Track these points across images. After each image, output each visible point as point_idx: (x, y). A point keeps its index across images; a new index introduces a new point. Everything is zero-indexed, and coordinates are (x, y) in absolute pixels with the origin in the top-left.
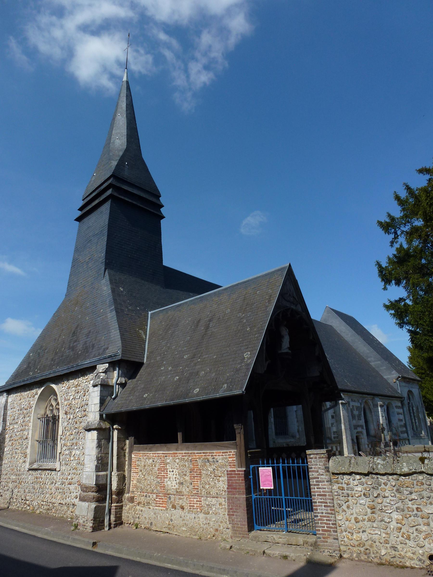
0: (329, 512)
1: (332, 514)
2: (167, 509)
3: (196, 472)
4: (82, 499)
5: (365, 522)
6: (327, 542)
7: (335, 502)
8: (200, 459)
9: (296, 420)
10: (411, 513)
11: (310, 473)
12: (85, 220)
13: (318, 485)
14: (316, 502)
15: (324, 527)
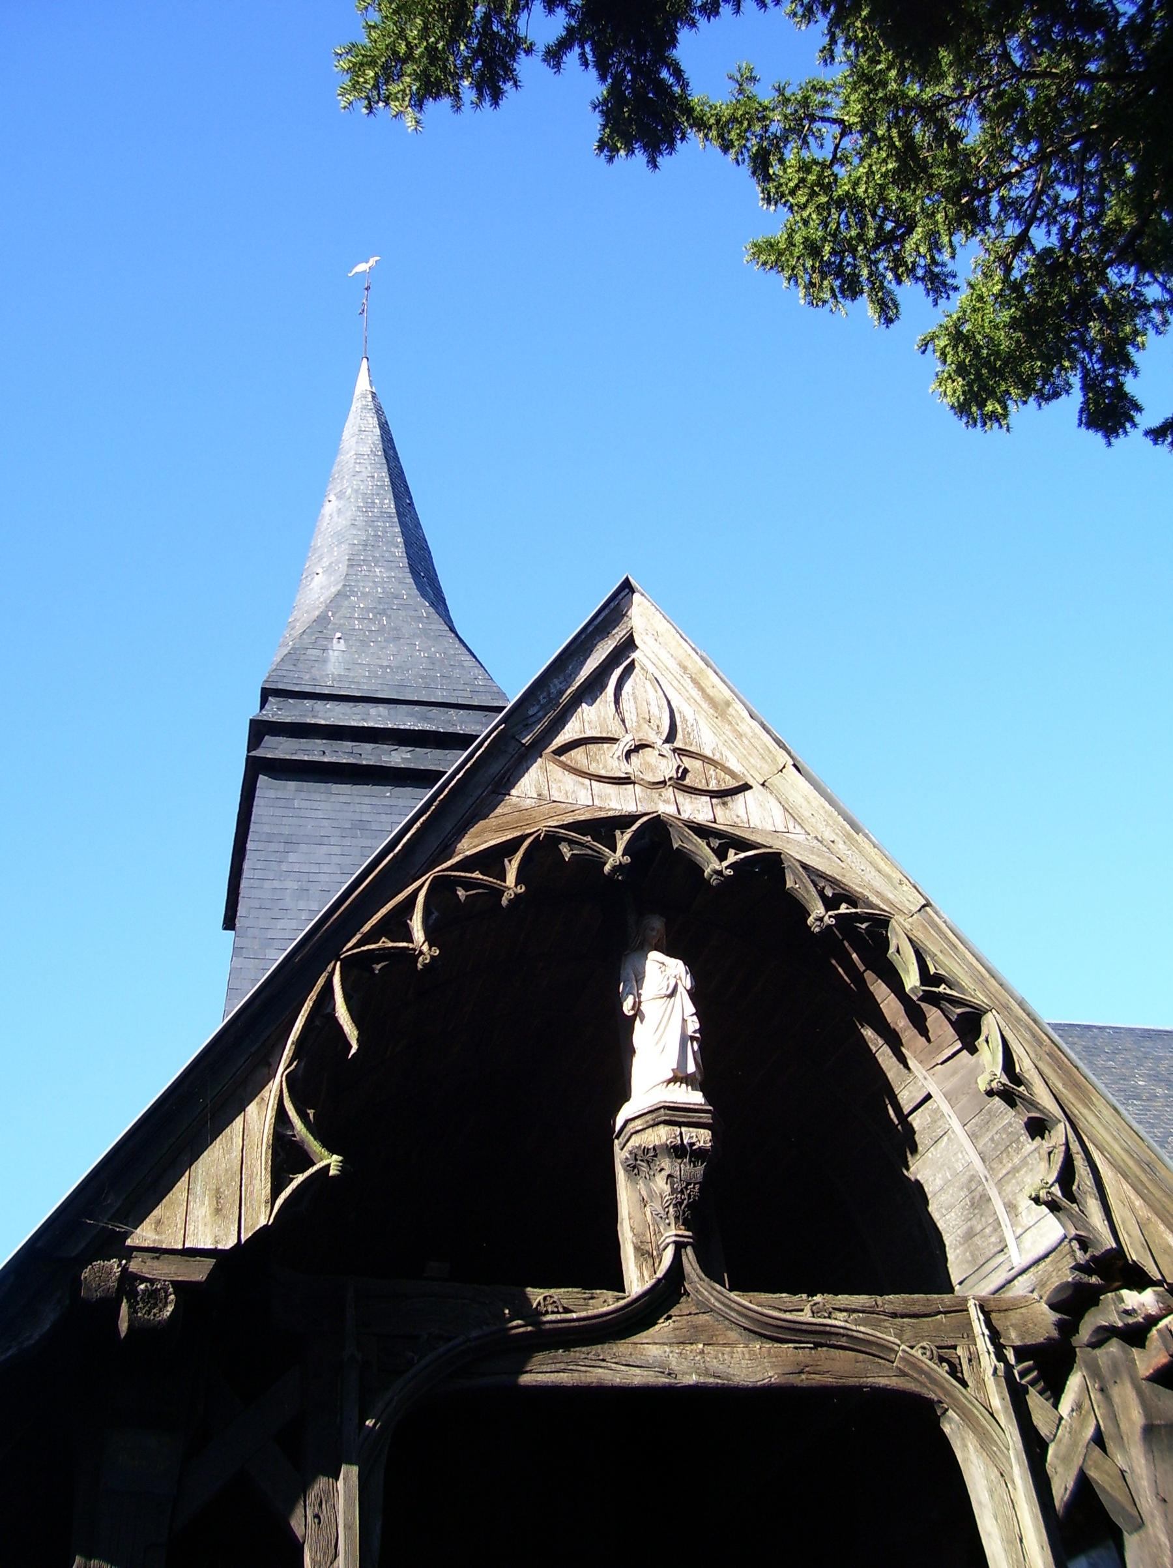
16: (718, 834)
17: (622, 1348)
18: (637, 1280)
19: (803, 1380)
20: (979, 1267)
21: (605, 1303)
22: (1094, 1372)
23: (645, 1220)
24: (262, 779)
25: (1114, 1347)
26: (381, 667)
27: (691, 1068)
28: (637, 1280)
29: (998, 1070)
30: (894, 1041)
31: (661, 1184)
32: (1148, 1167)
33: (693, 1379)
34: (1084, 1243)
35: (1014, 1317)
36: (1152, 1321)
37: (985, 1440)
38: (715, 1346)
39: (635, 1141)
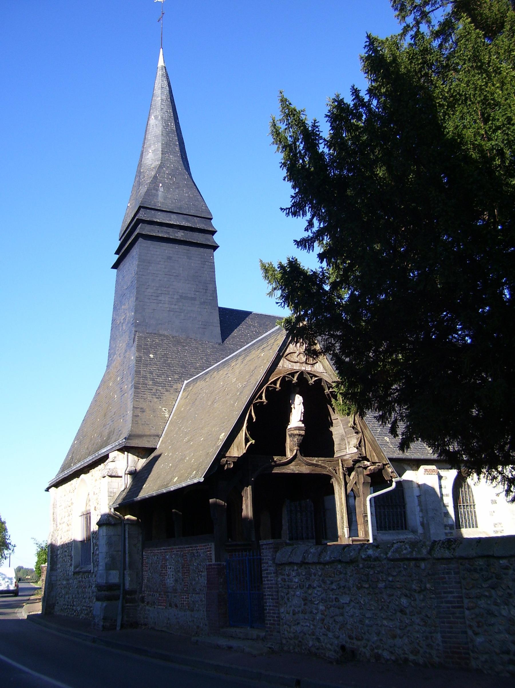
0: (275, 604)
1: (276, 606)
2: (166, 608)
3: (186, 568)
4: (98, 599)
5: (300, 614)
6: (272, 635)
7: (280, 594)
8: (188, 553)
9: (418, 509)
10: (331, 603)
11: (262, 565)
12: (121, 266)
13: (268, 577)
14: (265, 595)
15: (271, 620)
16: (312, 374)
17: (287, 466)
18: (289, 455)
19: (313, 472)
20: (340, 450)
21: (284, 460)
22: (357, 472)
23: (291, 447)
24: (140, 239)
25: (361, 469)
26: (174, 199)
27: (302, 419)
28: (289, 455)
29: (352, 423)
30: (333, 409)
31: (295, 439)
32: (373, 441)
33: (297, 472)
34: (360, 454)
35: (346, 462)
36: (368, 466)
37: (339, 483)
38: (300, 467)
39: (292, 432)
